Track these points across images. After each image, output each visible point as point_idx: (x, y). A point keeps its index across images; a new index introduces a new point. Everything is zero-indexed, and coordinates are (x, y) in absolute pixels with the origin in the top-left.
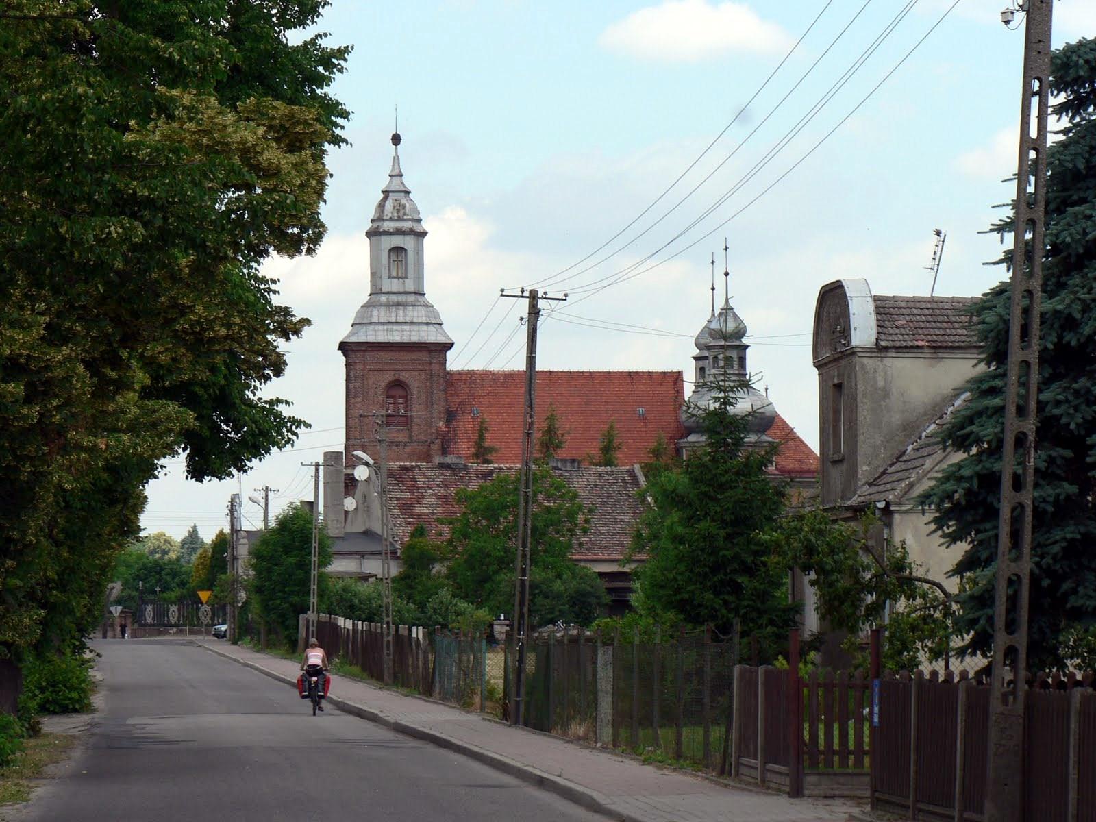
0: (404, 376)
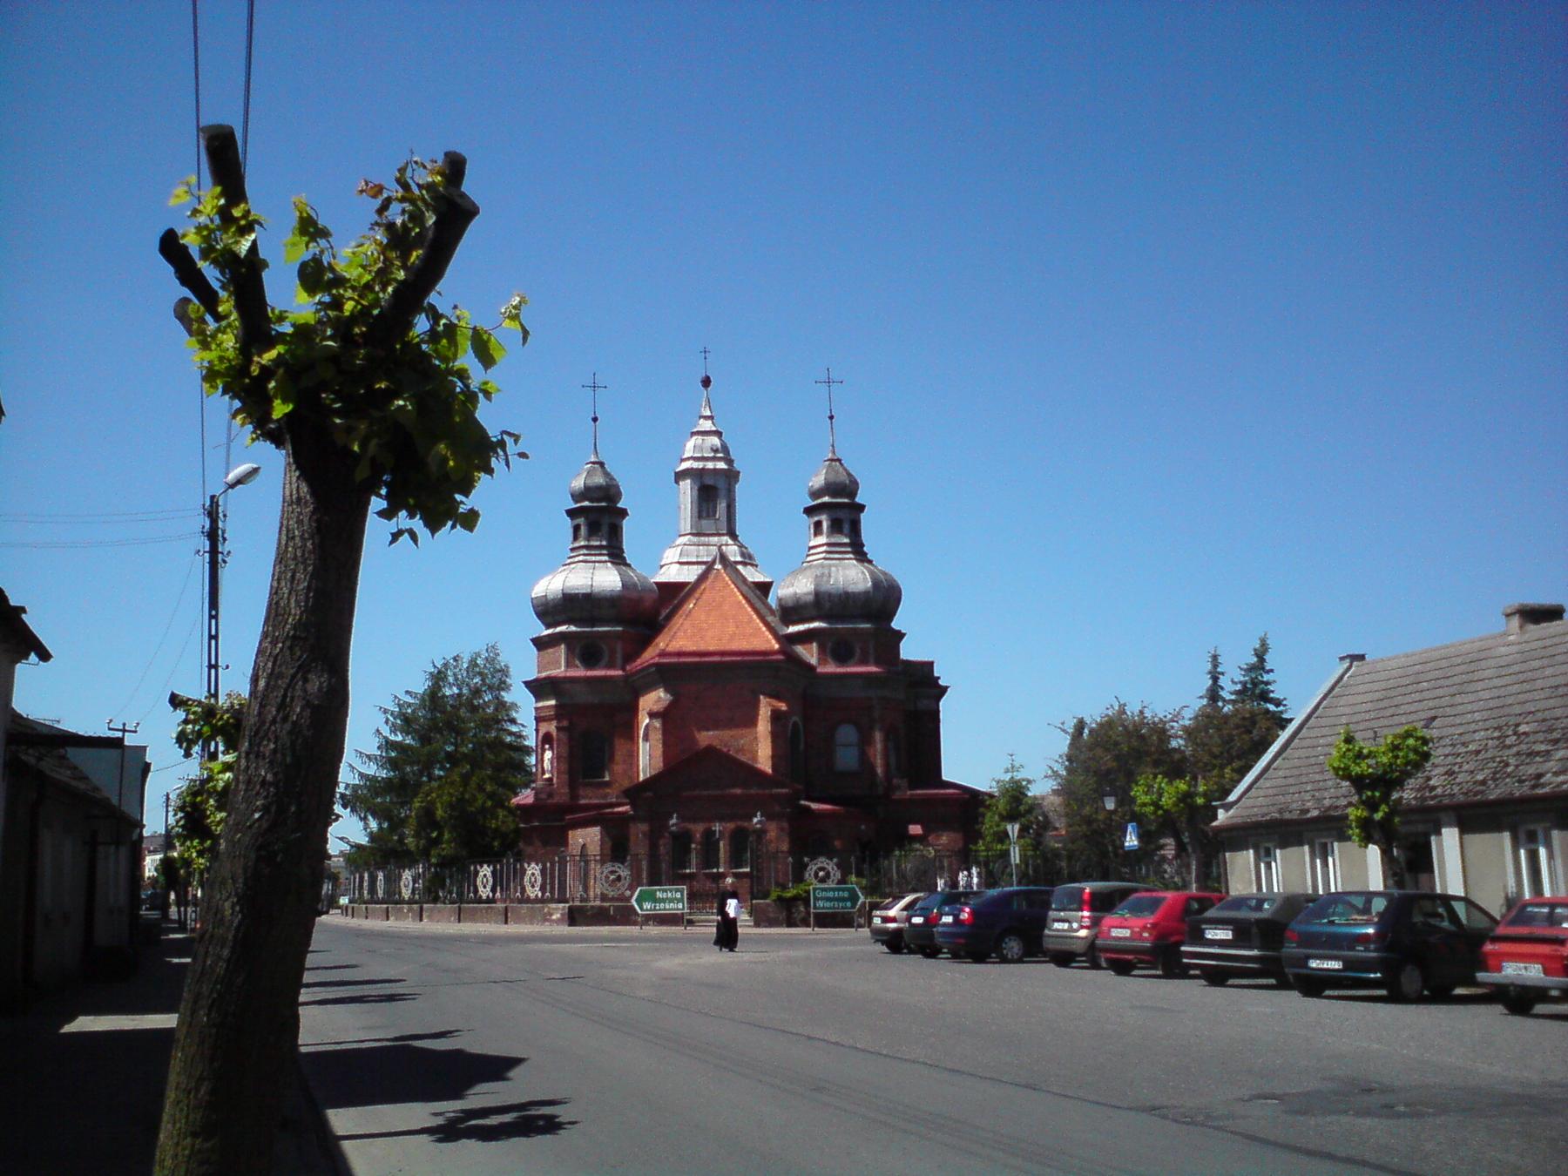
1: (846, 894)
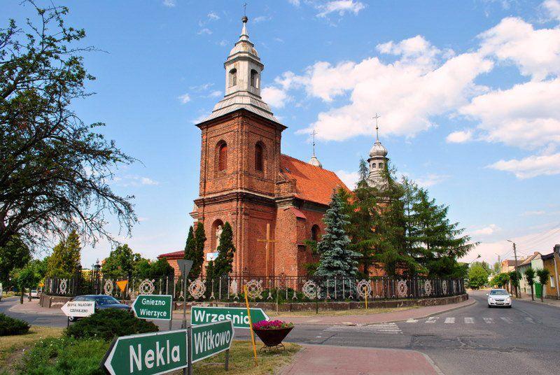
0: (264, 140)
1: (163, 303)
